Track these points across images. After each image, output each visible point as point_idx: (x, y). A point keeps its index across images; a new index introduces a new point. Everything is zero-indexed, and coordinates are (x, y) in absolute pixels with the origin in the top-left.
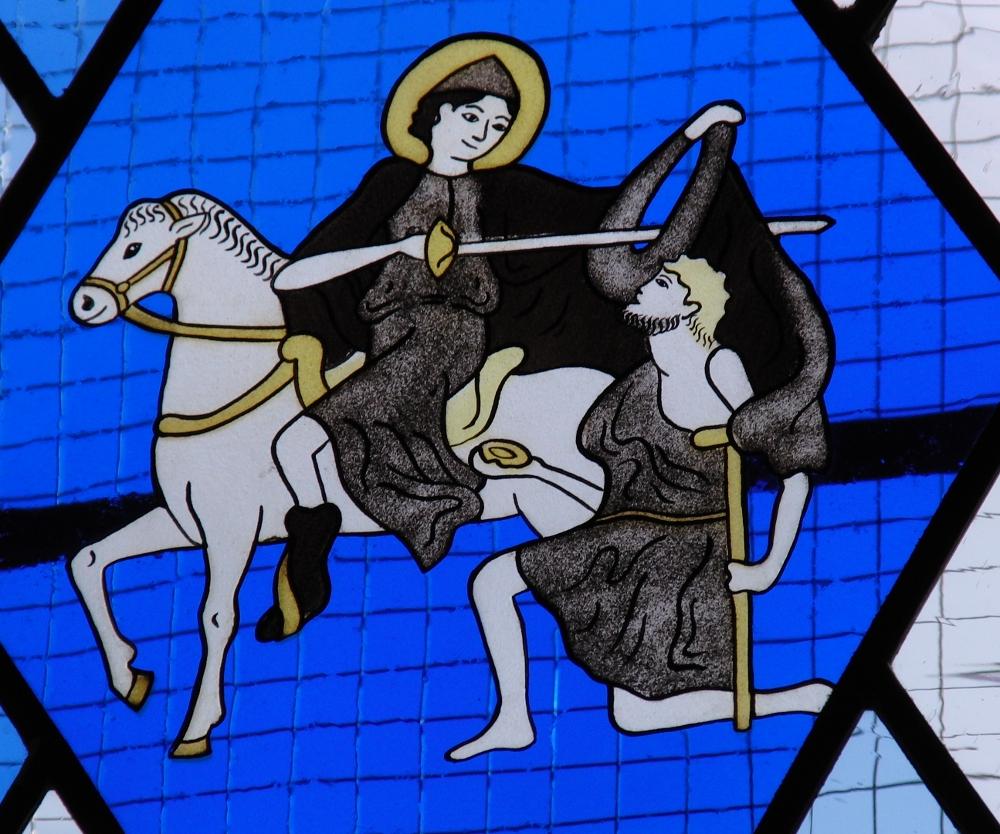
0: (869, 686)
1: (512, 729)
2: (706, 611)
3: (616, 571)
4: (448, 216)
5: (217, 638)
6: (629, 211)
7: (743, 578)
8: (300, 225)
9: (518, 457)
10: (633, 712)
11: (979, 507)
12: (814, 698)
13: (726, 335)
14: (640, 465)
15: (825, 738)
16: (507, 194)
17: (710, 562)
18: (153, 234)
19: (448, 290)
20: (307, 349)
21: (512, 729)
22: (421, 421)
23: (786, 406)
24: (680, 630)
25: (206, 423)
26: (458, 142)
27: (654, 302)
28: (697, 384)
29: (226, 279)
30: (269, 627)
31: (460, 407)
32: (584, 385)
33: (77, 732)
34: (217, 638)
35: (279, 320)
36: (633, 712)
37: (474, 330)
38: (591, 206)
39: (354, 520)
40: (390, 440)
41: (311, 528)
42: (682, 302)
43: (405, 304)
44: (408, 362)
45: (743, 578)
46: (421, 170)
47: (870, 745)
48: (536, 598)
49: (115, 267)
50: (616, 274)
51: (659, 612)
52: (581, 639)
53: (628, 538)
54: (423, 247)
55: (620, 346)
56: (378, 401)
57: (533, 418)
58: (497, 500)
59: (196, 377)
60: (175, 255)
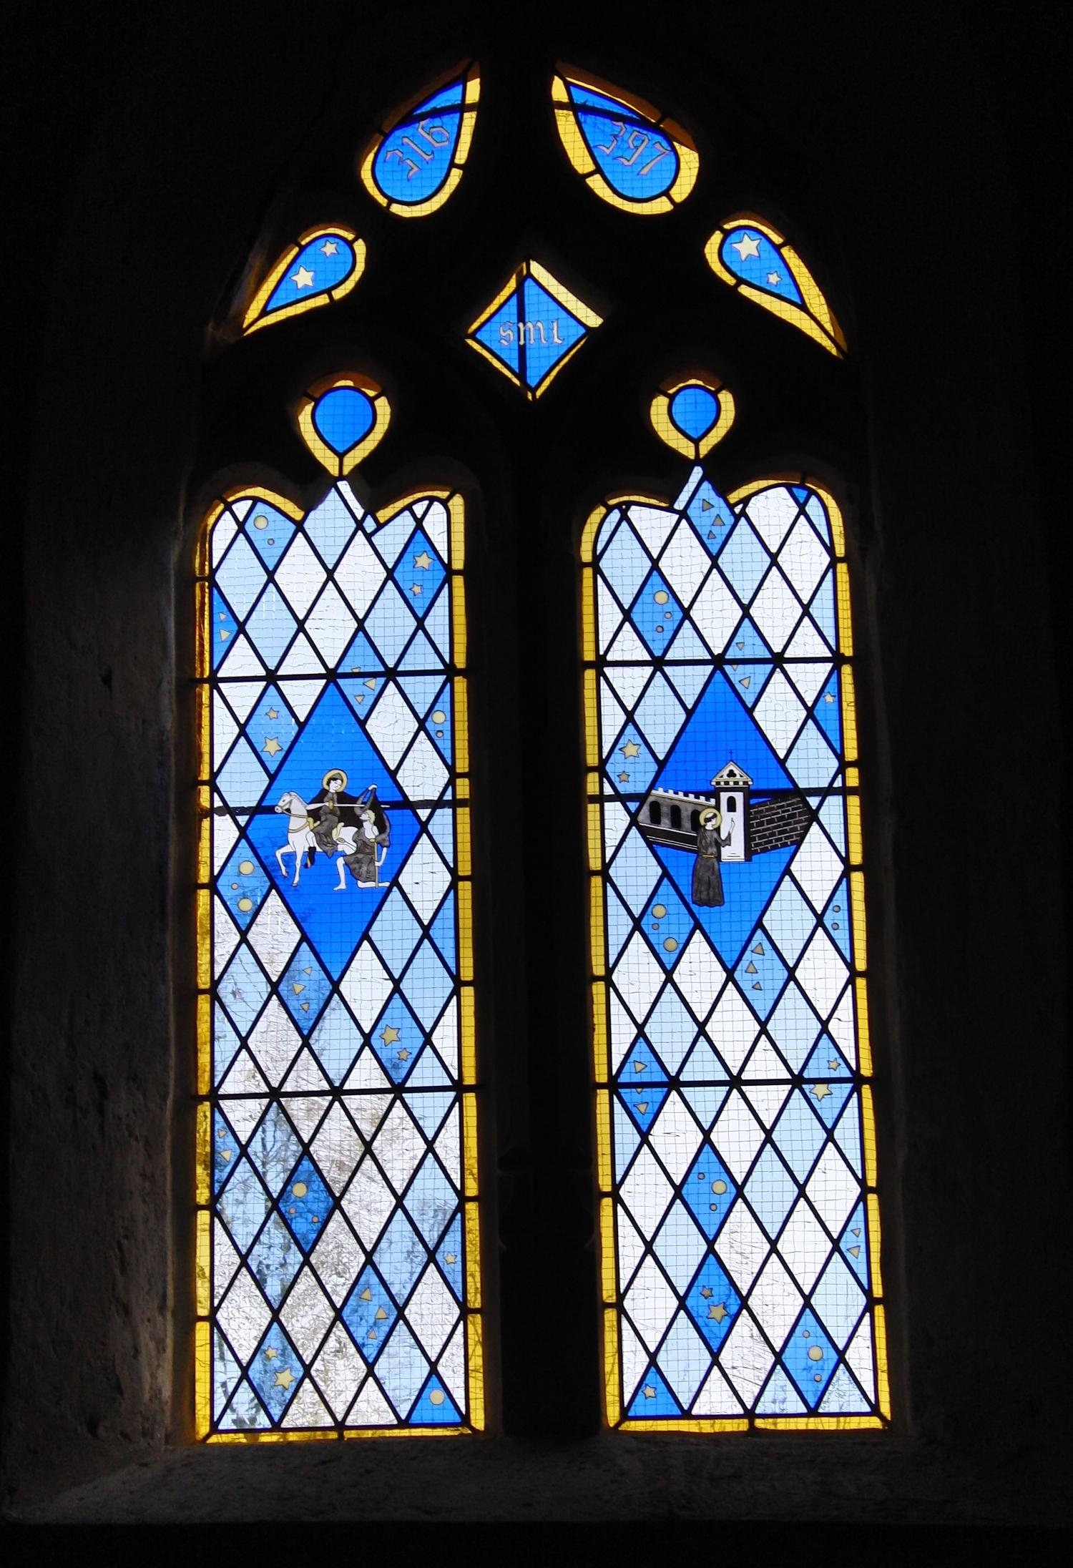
0: (395, 883)
1: (342, 886)
2: (372, 869)
3: (358, 861)
4: (332, 800)
5: (298, 867)
6: (360, 801)
7: (377, 864)
8: (313, 795)
9: (343, 840)
10: (361, 884)
11: (601, 1290)
12: (387, 884)
13: (375, 824)
14: (363, 846)
15: (389, 890)
16: (342, 797)
17: (372, 861)
18: (287, 798)
19: (332, 812)
20: (311, 820)
21: (342, 886)
22: (328, 834)
23: (384, 836)
24: (368, 872)
25: (296, 831)
26: (335, 787)
27: (363, 817)
28: (371, 832)
29: (299, 807)
30: (306, 866)
31: (334, 832)
32: (352, 830)
33: (278, 882)
34: (298, 867)
35: (333, 494)
36: (361, 884)
37: (336, 819)
38: (354, 800)
39: (318, 849)
40: (324, 836)
41: (312, 850)
42: (368, 817)
43: (326, 814)
44: (326, 824)
45: (377, 864)
46: (328, 791)
47: (395, 893)
48: (346, 864)
49: (281, 803)
50: (358, 812)
51: (365, 868)
52: (353, 874)
53: (360, 856)
54: (328, 804)
55: (359, 824)
56: (322, 830)
57: (345, 836)
58: (340, 848)
59: (294, 823)
60: (290, 802)
